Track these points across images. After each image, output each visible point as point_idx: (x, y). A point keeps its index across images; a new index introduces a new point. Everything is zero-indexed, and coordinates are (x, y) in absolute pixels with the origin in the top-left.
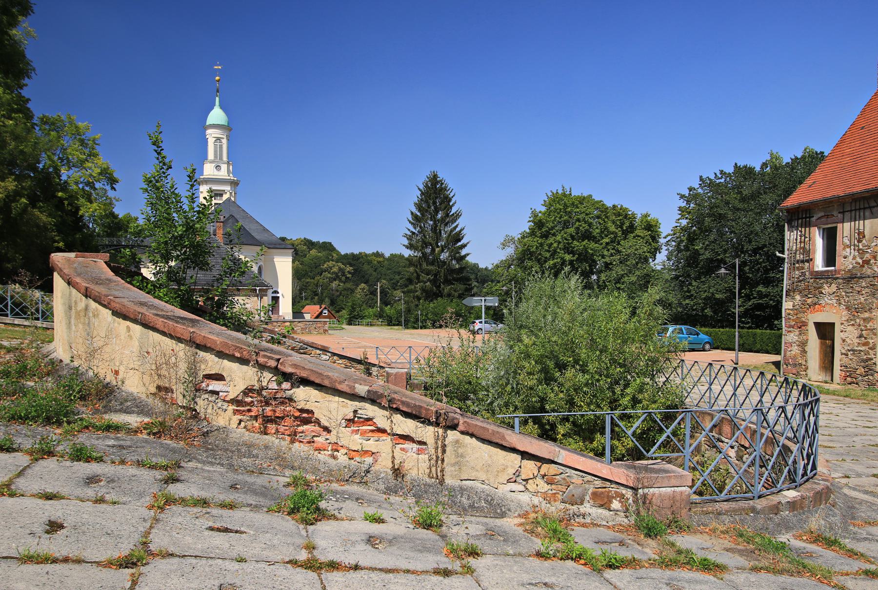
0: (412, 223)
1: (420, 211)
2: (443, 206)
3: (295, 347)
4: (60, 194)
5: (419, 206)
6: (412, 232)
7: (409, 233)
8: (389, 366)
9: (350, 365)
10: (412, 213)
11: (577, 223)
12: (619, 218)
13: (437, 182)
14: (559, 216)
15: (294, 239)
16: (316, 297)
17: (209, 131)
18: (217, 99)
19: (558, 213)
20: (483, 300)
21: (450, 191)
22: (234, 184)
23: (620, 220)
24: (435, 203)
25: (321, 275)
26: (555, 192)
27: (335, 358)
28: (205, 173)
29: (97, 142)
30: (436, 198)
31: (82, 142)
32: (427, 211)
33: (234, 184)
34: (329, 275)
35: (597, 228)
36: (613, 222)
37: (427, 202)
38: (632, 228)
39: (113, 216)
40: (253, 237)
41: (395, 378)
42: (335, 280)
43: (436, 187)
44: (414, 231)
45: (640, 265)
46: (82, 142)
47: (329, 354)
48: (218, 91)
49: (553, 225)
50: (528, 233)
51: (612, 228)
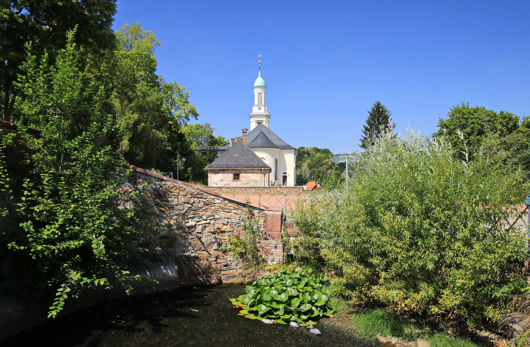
0: (365, 133)
1: (369, 125)
2: (384, 121)
3: (193, 193)
4: (170, 122)
5: (369, 123)
6: (364, 138)
7: (363, 138)
8: (267, 209)
9: (237, 207)
10: (364, 127)
11: (472, 125)
12: (505, 120)
13: (380, 108)
14: (459, 121)
15: (309, 148)
16: (319, 179)
17: (255, 90)
18: (259, 72)
19: (458, 119)
20: (347, 158)
21: (388, 112)
22: (268, 117)
23: (506, 121)
24: (378, 120)
25: (322, 166)
26: (456, 106)
27: (226, 202)
28: (253, 112)
29: (188, 96)
30: (379, 117)
31: (181, 96)
32: (373, 125)
33: (268, 117)
34: (326, 167)
35: (488, 128)
36: (501, 123)
37: (373, 119)
38: (515, 126)
39: (212, 137)
40: (272, 143)
41: (272, 219)
42: (330, 169)
43: (379, 110)
44: (366, 137)
45: (521, 150)
46: (181, 96)
47: (222, 199)
48: (260, 68)
49: (454, 127)
50: (438, 134)
51: (500, 127)
